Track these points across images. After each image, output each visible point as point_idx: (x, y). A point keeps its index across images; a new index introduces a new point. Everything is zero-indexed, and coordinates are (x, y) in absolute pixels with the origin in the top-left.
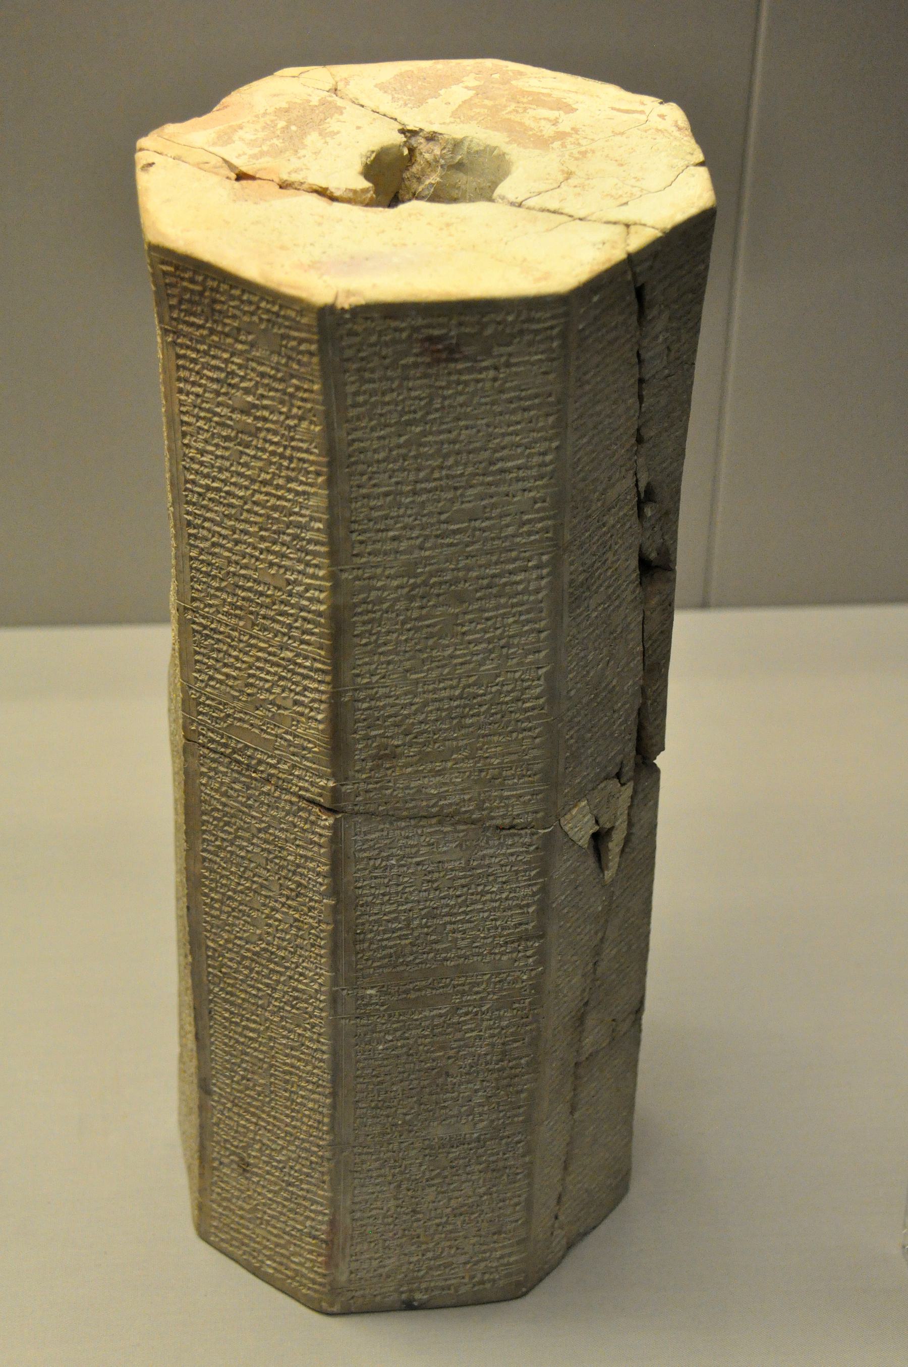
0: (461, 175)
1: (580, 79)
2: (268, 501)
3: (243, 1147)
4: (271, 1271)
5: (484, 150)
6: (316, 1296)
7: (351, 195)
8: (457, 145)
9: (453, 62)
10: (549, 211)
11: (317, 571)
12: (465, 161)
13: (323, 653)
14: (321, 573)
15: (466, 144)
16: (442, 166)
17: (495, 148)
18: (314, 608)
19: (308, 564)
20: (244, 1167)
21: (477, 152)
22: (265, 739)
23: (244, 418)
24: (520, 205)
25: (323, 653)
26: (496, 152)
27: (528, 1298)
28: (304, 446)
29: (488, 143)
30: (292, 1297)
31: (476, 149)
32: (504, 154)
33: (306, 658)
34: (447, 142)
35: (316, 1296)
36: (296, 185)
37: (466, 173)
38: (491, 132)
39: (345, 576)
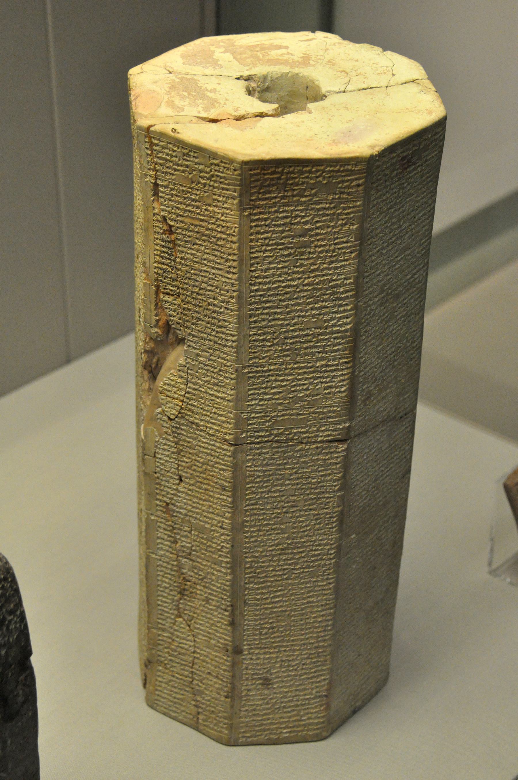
0: (268, 93)
1: (260, 34)
2: (315, 281)
3: (267, 672)
4: (287, 735)
5: (282, 76)
6: (318, 731)
7: (274, 112)
8: (265, 77)
9: (192, 44)
10: (363, 89)
11: (346, 308)
12: (270, 85)
13: (347, 352)
14: (349, 308)
15: (270, 76)
16: (259, 92)
17: (288, 73)
18: (343, 329)
19: (340, 306)
20: (267, 682)
21: (277, 78)
22: (301, 419)
23: (302, 239)
24: (344, 92)
25: (347, 352)
26: (290, 75)
27: (391, 678)
28: (345, 240)
29: (283, 71)
30: (306, 742)
31: (276, 76)
32: (297, 74)
33: (334, 360)
34: (259, 78)
35: (318, 731)
36: (246, 116)
37: (270, 92)
38: (272, 67)
39: (360, 304)
